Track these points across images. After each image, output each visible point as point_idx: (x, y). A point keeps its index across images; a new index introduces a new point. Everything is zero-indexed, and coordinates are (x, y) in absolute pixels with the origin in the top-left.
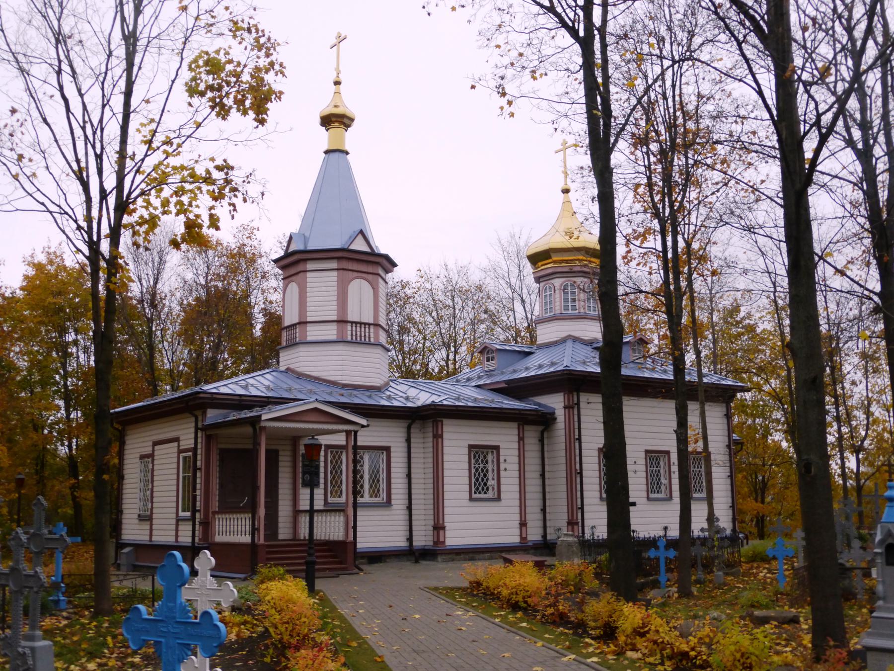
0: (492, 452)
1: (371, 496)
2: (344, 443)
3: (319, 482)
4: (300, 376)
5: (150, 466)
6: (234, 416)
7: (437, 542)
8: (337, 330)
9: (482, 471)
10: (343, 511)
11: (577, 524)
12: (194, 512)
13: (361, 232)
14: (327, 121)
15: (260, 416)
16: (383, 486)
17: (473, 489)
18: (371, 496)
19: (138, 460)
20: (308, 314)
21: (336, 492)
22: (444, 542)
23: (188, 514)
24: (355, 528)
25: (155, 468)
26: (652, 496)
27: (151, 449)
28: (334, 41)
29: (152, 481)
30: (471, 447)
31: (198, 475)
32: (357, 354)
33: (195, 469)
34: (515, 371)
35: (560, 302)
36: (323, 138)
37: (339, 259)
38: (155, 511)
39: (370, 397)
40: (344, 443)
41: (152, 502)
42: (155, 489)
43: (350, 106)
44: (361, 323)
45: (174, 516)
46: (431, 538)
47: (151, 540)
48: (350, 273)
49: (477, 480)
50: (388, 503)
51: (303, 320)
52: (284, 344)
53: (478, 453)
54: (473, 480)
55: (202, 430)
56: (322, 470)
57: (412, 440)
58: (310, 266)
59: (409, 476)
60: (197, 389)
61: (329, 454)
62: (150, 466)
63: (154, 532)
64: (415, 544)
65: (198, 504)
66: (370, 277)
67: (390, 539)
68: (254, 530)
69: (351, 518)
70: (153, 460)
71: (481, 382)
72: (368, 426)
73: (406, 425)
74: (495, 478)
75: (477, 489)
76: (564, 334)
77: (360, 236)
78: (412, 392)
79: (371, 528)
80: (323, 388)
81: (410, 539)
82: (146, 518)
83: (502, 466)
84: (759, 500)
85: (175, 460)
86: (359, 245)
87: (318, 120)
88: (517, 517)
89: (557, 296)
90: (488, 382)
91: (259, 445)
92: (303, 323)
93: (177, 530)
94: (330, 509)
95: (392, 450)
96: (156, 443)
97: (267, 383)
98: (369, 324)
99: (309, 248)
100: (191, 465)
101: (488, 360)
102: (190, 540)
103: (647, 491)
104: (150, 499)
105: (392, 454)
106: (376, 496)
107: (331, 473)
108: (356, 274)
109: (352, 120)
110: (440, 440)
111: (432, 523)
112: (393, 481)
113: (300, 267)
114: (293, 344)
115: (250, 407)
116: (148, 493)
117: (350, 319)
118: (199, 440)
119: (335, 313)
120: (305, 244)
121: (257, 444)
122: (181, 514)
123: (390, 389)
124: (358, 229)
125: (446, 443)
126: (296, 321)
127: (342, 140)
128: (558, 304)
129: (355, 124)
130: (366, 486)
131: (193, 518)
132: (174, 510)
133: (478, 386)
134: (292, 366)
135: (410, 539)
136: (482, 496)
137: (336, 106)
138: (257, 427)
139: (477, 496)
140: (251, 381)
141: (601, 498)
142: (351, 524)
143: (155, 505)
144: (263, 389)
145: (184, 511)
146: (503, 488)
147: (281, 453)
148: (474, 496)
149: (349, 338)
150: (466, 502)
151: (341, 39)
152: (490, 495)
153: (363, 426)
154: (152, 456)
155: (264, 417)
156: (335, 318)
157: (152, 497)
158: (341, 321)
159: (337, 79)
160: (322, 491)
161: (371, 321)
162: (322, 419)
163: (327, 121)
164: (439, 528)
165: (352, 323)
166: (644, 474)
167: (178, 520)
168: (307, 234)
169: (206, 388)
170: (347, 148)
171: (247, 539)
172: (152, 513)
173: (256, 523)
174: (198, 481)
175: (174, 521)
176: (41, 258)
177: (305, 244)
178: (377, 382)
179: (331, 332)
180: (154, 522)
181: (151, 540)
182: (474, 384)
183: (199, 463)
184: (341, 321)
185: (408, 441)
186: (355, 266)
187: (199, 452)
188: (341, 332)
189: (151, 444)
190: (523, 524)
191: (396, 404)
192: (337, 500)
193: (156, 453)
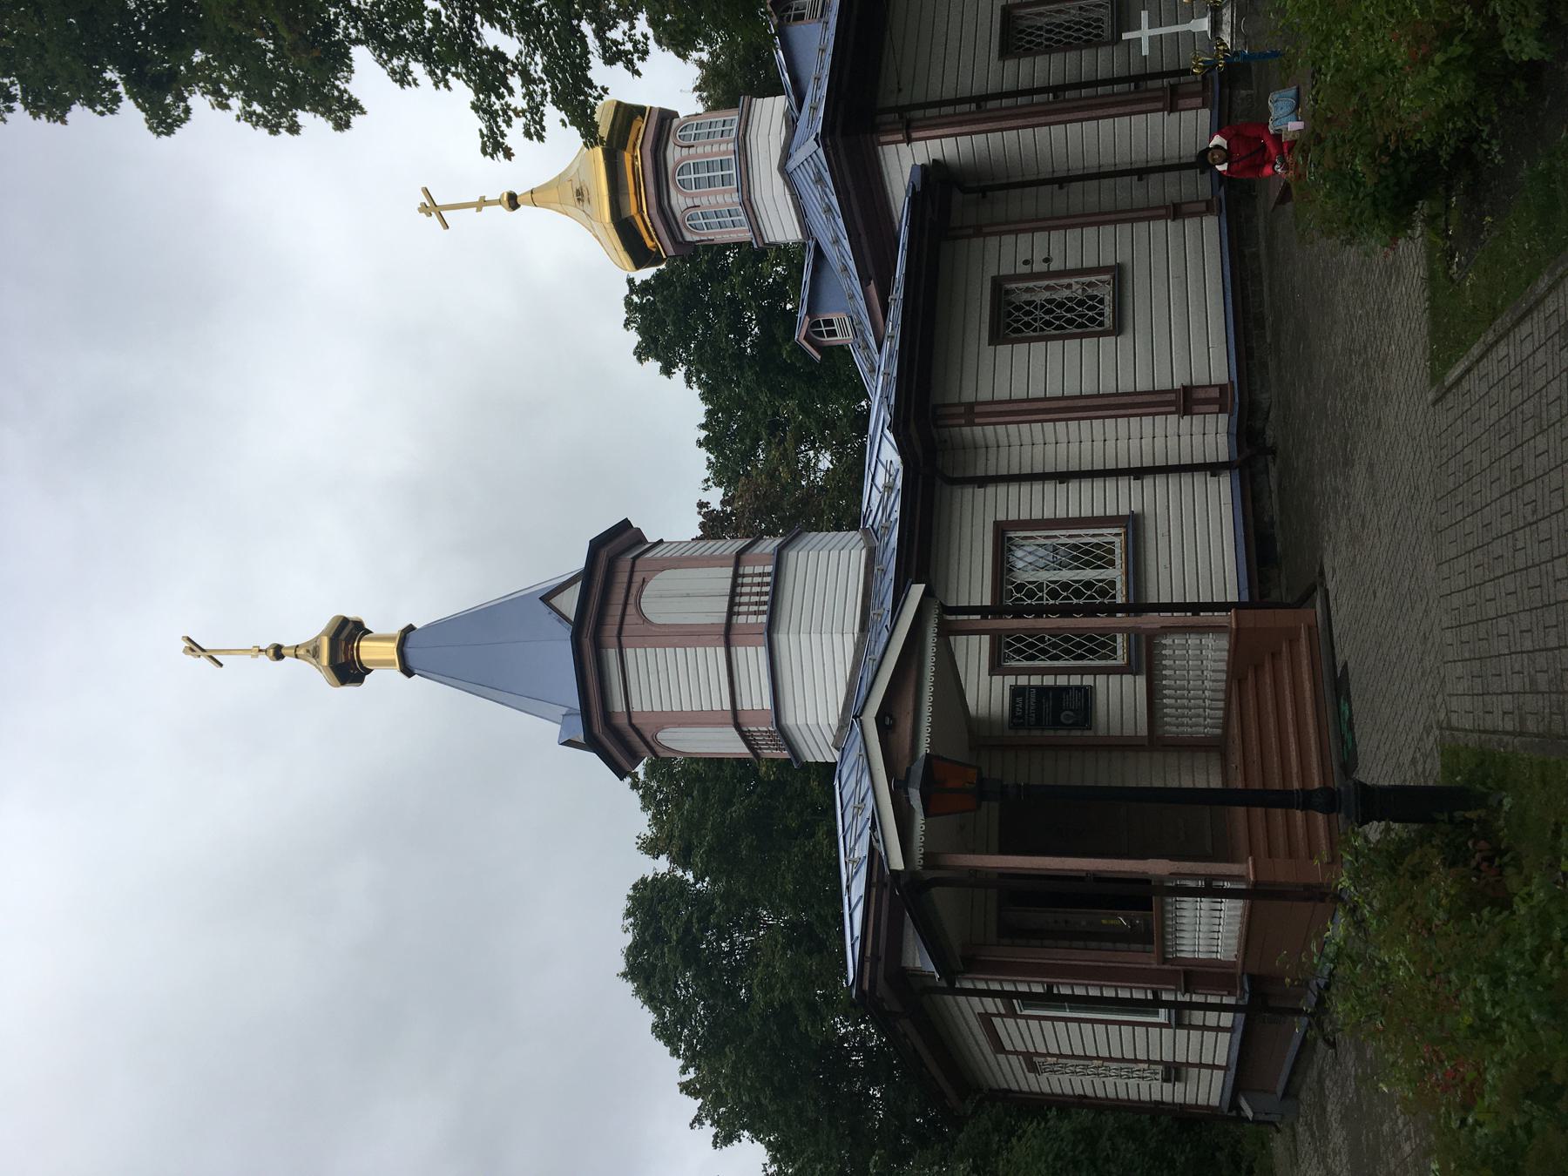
0: (1008, 292)
1: (1112, 563)
2: (986, 639)
3: (1079, 688)
7: (1219, 399)
8: (746, 646)
9: (1049, 312)
11: (1173, 88)
14: (348, 671)
16: (1086, 536)
18: (1112, 563)
20: (716, 707)
21: (1103, 645)
22: (1222, 388)
24: (1196, 608)
31: (1065, 991)
34: (845, 269)
35: (716, 193)
36: (385, 680)
37: (599, 647)
40: (986, 639)
46: (1210, 419)
48: (628, 619)
50: (1133, 525)
51: (730, 716)
52: (785, 754)
56: (1049, 680)
57: (980, 472)
58: (618, 706)
59: (1063, 477)
61: (1014, 663)
63: (1207, 1059)
64: (1224, 457)
65: (1138, 995)
66: (637, 578)
67: (1214, 514)
68: (1211, 891)
69: (1165, 618)
70: (1037, 1054)
74: (1065, 281)
75: (1092, 320)
76: (778, 180)
81: (1214, 469)
83: (1039, 267)
84: (1143, 638)
86: (569, 602)
87: (349, 690)
88: (1158, 226)
89: (704, 200)
91: (974, 871)
92: (736, 718)
94: (1145, 660)
95: (1001, 517)
98: (736, 575)
101: (832, 333)
105: (1013, 516)
106: (1112, 552)
108: (631, 610)
110: (978, 409)
111: (1173, 418)
112: (1073, 513)
113: (622, 722)
114: (783, 735)
117: (722, 619)
118: (982, 986)
121: (976, 878)
125: (984, 395)
128: (720, 199)
130: (1089, 574)
132: (1154, 1031)
134: (830, 740)
135: (1214, 469)
136: (1108, 311)
137: (315, 653)
138: (930, 875)
146: (1090, 262)
148: (1108, 323)
149: (763, 619)
150: (1124, 341)
151: (194, 648)
152: (1106, 292)
156: (721, 651)
158: (728, 635)
160: (1101, 679)
161: (729, 571)
164: (1186, 401)
165: (731, 613)
168: (564, 710)
172: (1161, 1062)
173: (1191, 884)
176: (708, 1130)
178: (858, 557)
179: (751, 659)
180: (1180, 1058)
182: (877, 356)
184: (728, 635)
186: (615, 610)
189: (1001, 1057)
190: (1176, 212)
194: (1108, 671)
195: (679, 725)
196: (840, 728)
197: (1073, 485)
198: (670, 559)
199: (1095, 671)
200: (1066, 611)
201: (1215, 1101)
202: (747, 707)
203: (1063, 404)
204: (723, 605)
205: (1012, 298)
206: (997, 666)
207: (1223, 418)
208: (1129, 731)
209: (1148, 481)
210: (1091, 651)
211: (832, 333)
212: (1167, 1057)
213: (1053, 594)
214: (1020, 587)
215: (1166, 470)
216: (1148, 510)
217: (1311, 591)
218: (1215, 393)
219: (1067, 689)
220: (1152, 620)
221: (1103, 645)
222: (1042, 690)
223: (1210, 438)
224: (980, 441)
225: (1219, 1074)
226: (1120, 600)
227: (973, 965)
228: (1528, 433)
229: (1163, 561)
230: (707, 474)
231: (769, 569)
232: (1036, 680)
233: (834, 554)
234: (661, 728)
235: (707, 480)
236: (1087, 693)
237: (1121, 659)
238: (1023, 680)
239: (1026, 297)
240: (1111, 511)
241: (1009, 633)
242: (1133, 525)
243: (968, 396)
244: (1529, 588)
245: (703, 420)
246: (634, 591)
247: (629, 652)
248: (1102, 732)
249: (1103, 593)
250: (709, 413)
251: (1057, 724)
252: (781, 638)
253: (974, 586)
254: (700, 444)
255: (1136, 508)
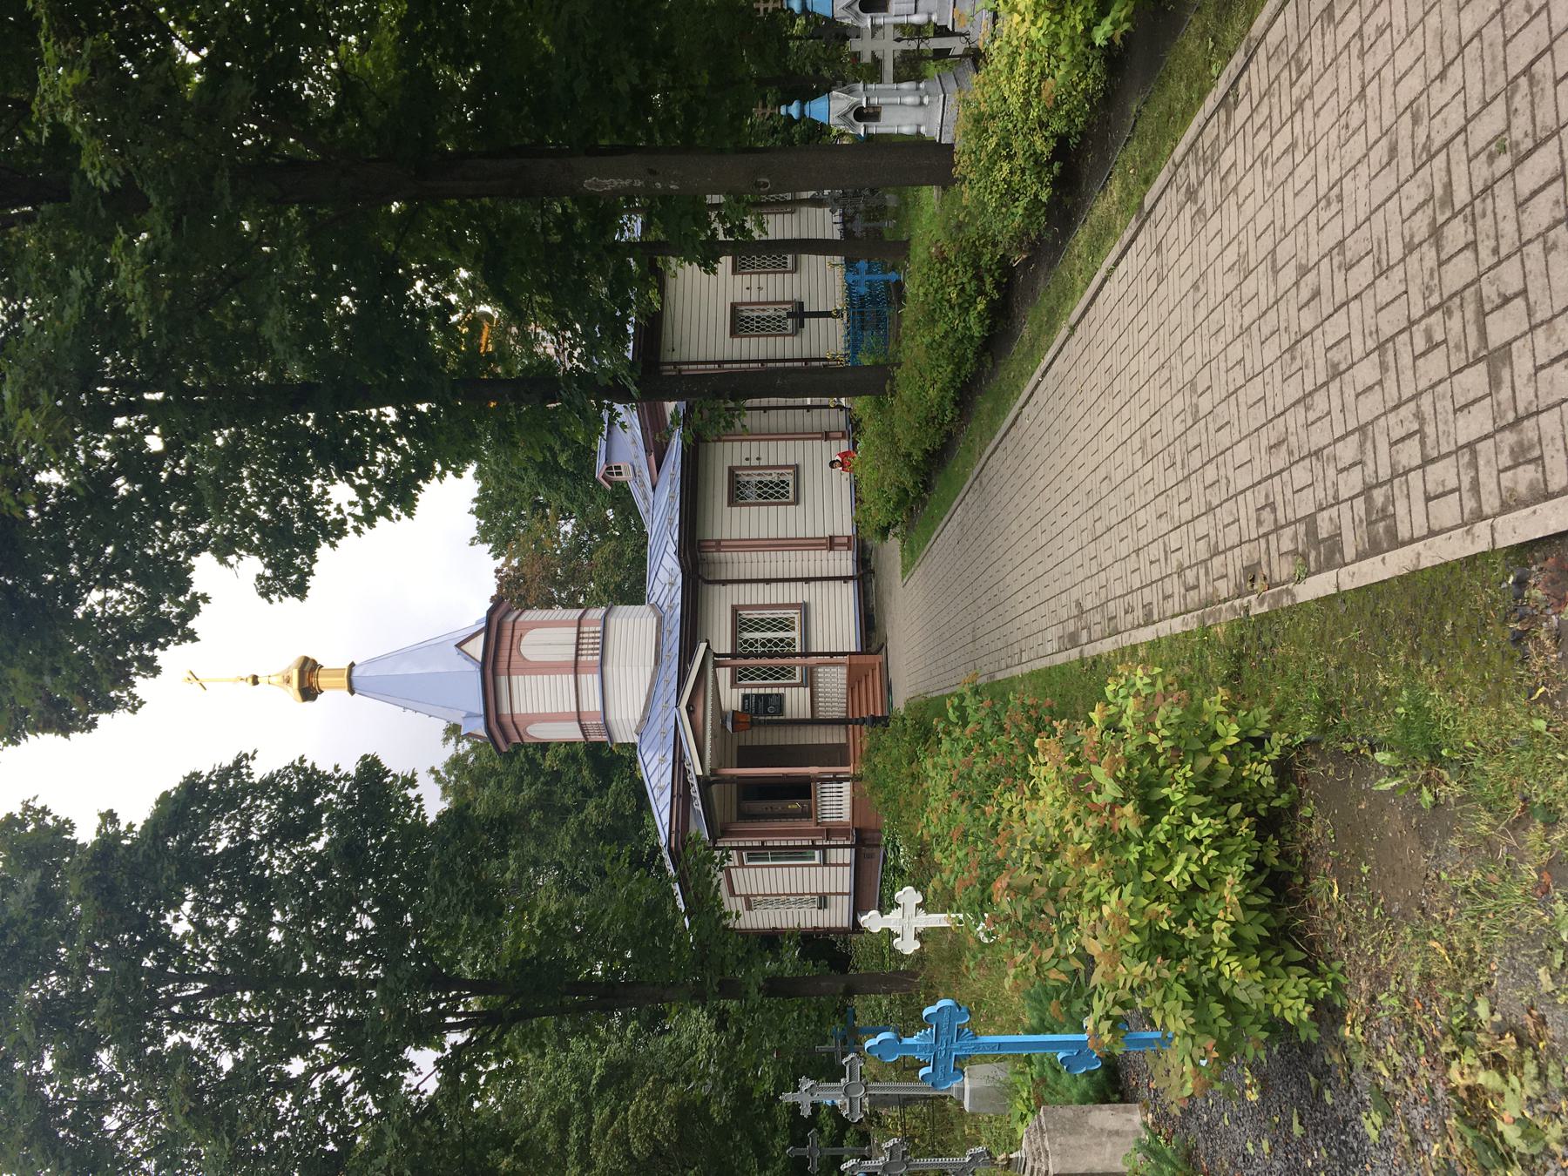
1: (793, 629)
2: (728, 669)
4: (646, 718)
5: (759, 898)
6: (698, 805)
10: (811, 669)
12: (814, 847)
13: (459, 646)
14: (309, 693)
15: (698, 777)
16: (779, 614)
17: (784, 500)
18: (793, 629)
19: (752, 913)
20: (567, 710)
21: (789, 672)
22: (849, 537)
23: (817, 853)
24: (831, 654)
25: (761, 892)
26: (790, 266)
27: (738, 899)
28: (196, 684)
29: (778, 895)
30: (731, 503)
32: (616, 652)
33: (763, 847)
36: (333, 697)
37: (495, 674)
38: (813, 891)
39: (671, 632)
40: (728, 669)
41: (804, 894)
42: (787, 891)
43: (289, 662)
44: (578, 644)
45: (819, 869)
47: (849, 894)
49: (771, 495)
50: (804, 608)
52: (605, 738)
53: (737, 495)
54: (772, 500)
55: (715, 842)
56: (762, 691)
57: (723, 578)
58: (505, 710)
60: (665, 853)
62: (759, 898)
63: (840, 890)
64: (850, 574)
65: (805, 843)
66: (517, 633)
70: (752, 895)
71: (649, 485)
72: (707, 641)
73: (705, 586)
75: (783, 495)
77: (465, 647)
78: (663, 576)
79: (832, 596)
80: (660, 690)
81: (845, 579)
82: (823, 901)
83: (754, 463)
85: (752, 870)
86: (476, 648)
87: (308, 703)
88: (817, 443)
90: (647, 474)
91: (733, 776)
93: (837, 865)
94: (809, 680)
96: (732, 893)
97: (655, 762)
98: (579, 633)
99: (480, 710)
100: (757, 854)
101: (620, 474)
102: (848, 851)
103: (784, 273)
104: (799, 898)
105: (741, 603)
107: (765, 679)
108: (514, 652)
109: (306, 659)
111: (825, 552)
112: (774, 602)
113: (507, 721)
115: (687, 786)
116: (792, 899)
119: (564, 677)
120: (478, 716)
122: (817, 861)
123: (660, 603)
124: (454, 650)
125: (726, 536)
126: (576, 725)
127: (335, 672)
129: (311, 656)
130: (781, 634)
131: (824, 848)
132: (813, 869)
133: (654, 488)
134: (634, 729)
135: (845, 579)
136: (791, 490)
137: (288, 681)
139: (791, 497)
140: (654, 781)
141: (792, 213)
142: (827, 658)
143: (807, 891)
144: (666, 765)
145: (813, 858)
146: (782, 462)
147: (742, 744)
149: (597, 658)
150: (800, 508)
152: (790, 479)
153: (708, 647)
154: (747, 898)
155: (700, 773)
156: (571, 677)
157: (797, 894)
158: (576, 668)
159: (250, 680)
161: (574, 630)
162: (702, 689)
163: (309, 693)
164: (831, 543)
165: (577, 655)
166: (763, 277)
167: (825, 863)
168: (464, 714)
169: (663, 841)
170: (346, 666)
171: (847, 786)
172: (817, 894)
174: (776, 844)
175: (826, 869)
177: (478, 716)
178: (652, 622)
179: (590, 682)
180: (827, 891)
181: (849, 894)
183: (756, 844)
184: (576, 668)
185: (725, 582)
186: (505, 653)
187: (741, 844)
188: (589, 668)
189: (732, 899)
191: (678, 600)
192: (798, 641)
193: (744, 893)
194: (792, 686)
195: (544, 721)
196: (641, 721)
197: (774, 585)
198: (536, 622)
199: (785, 686)
200: (771, 656)
201: (846, 925)
202: (585, 709)
203: (768, 542)
204: (573, 650)
205: (740, 479)
206: (734, 684)
207: (850, 553)
208: (802, 716)
209: (812, 584)
210: (784, 676)
211: (620, 474)
212: (820, 891)
213: (763, 645)
214: (746, 641)
215: (822, 579)
216: (812, 602)
217: (882, 647)
218: (845, 540)
219: (771, 695)
220: (813, 660)
221: (789, 672)
222: (758, 696)
223: (844, 562)
224: (723, 560)
225: (846, 898)
226: (798, 650)
227: (726, 833)
228: (1138, 464)
229: (820, 628)
230: (475, 533)
231: (599, 629)
232: (755, 691)
233: (637, 620)
234: (531, 723)
235: (474, 539)
236: (781, 697)
237: (798, 680)
238: (748, 691)
239: (747, 479)
240: (793, 601)
241: (740, 666)
242: (804, 608)
243: (717, 537)
244: (1226, 576)
245: (477, 495)
246: (515, 641)
247: (514, 678)
248: (788, 716)
249: (789, 645)
250: (482, 490)
251: (766, 713)
252: (608, 669)
253: (722, 641)
254: (471, 512)
255: (806, 600)
